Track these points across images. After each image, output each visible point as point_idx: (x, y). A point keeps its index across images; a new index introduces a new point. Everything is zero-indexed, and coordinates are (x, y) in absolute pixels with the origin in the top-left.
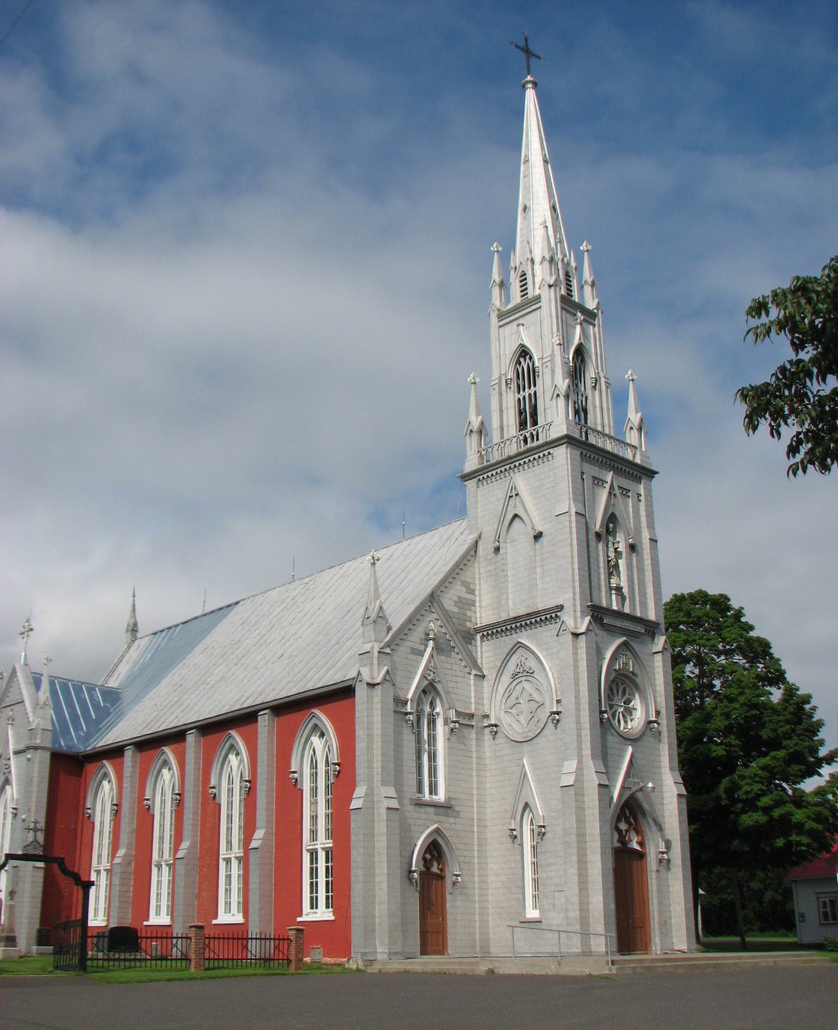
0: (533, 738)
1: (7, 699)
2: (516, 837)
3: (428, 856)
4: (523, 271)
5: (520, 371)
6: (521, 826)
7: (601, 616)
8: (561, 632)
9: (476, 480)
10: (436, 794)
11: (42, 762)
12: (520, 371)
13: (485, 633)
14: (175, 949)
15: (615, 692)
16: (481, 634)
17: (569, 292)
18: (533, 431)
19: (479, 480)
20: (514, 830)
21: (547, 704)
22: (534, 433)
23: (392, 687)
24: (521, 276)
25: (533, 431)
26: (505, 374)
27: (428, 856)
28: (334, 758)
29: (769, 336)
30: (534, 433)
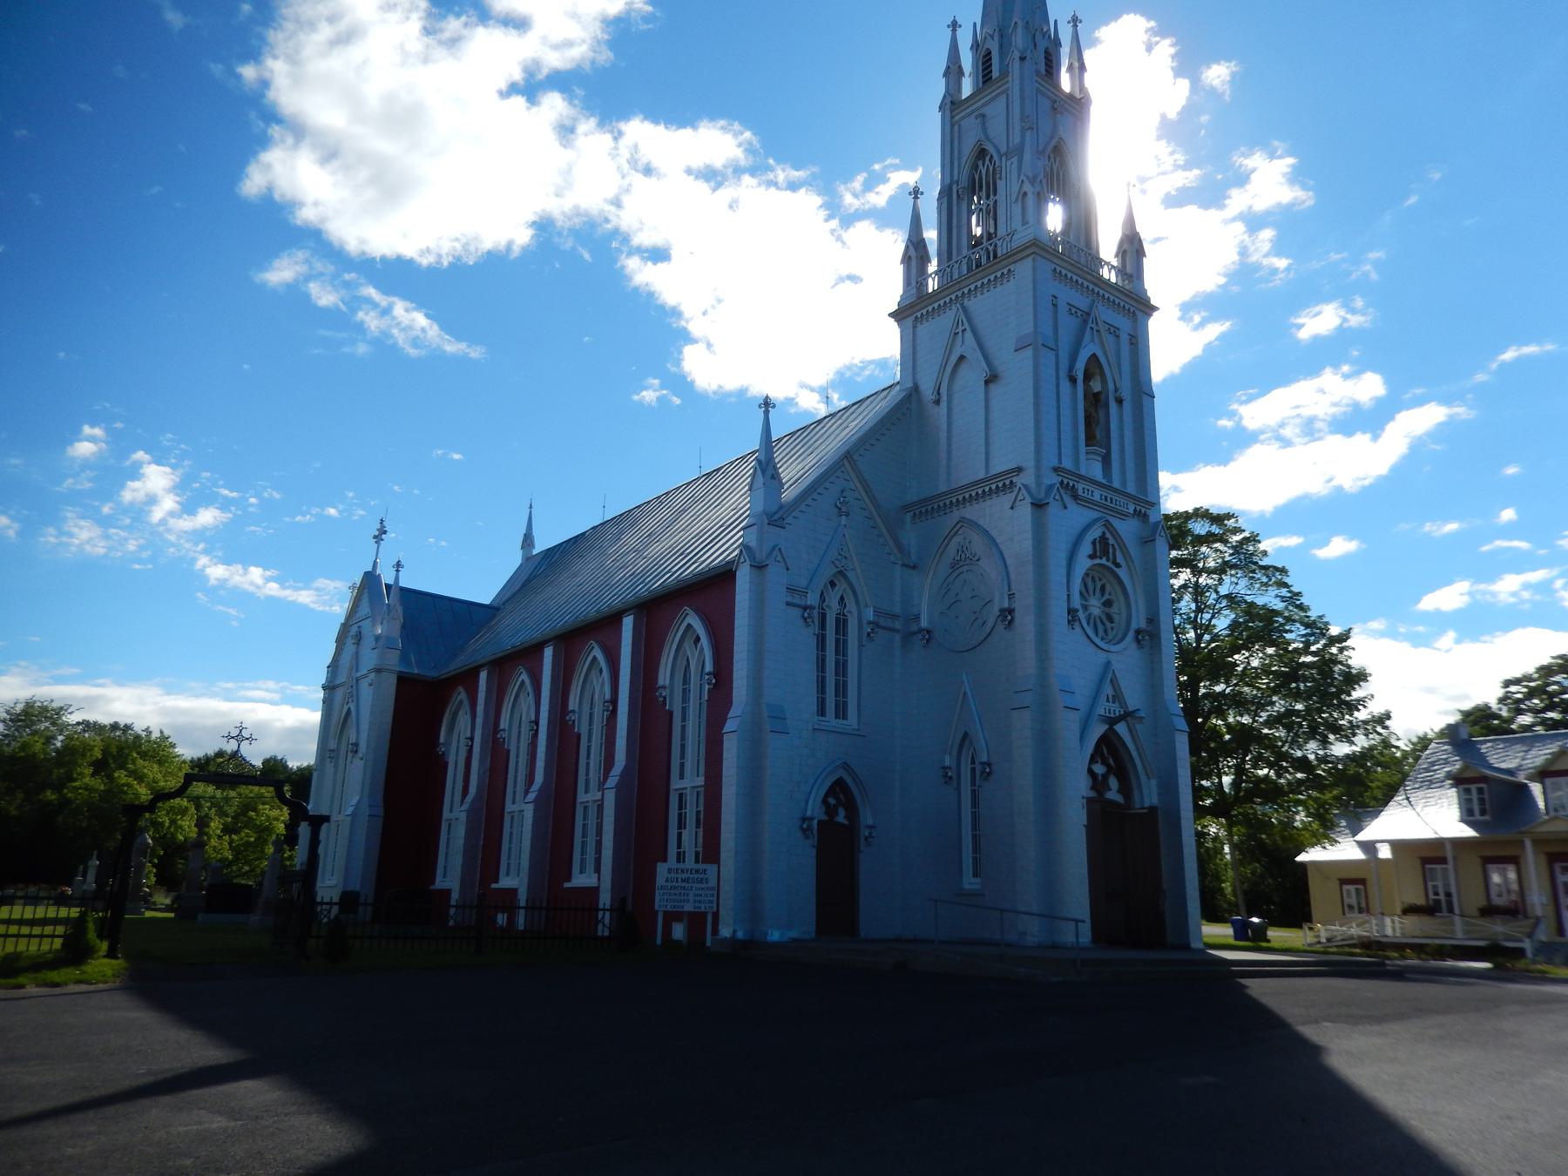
0: (975, 647)
1: (358, 615)
2: (951, 778)
3: (832, 801)
4: (988, 49)
5: (977, 178)
6: (959, 764)
7: (1074, 485)
8: (1018, 503)
9: (913, 318)
10: (847, 719)
11: (390, 683)
12: (977, 178)
13: (917, 512)
14: (600, 927)
15: (1091, 592)
16: (912, 514)
17: (1048, 69)
18: (989, 247)
19: (916, 317)
20: (950, 768)
21: (996, 600)
22: (991, 248)
23: (785, 571)
24: (984, 57)
25: (989, 247)
26: (957, 182)
27: (832, 801)
28: (709, 667)
29: (1291, 586)
30: (991, 248)
